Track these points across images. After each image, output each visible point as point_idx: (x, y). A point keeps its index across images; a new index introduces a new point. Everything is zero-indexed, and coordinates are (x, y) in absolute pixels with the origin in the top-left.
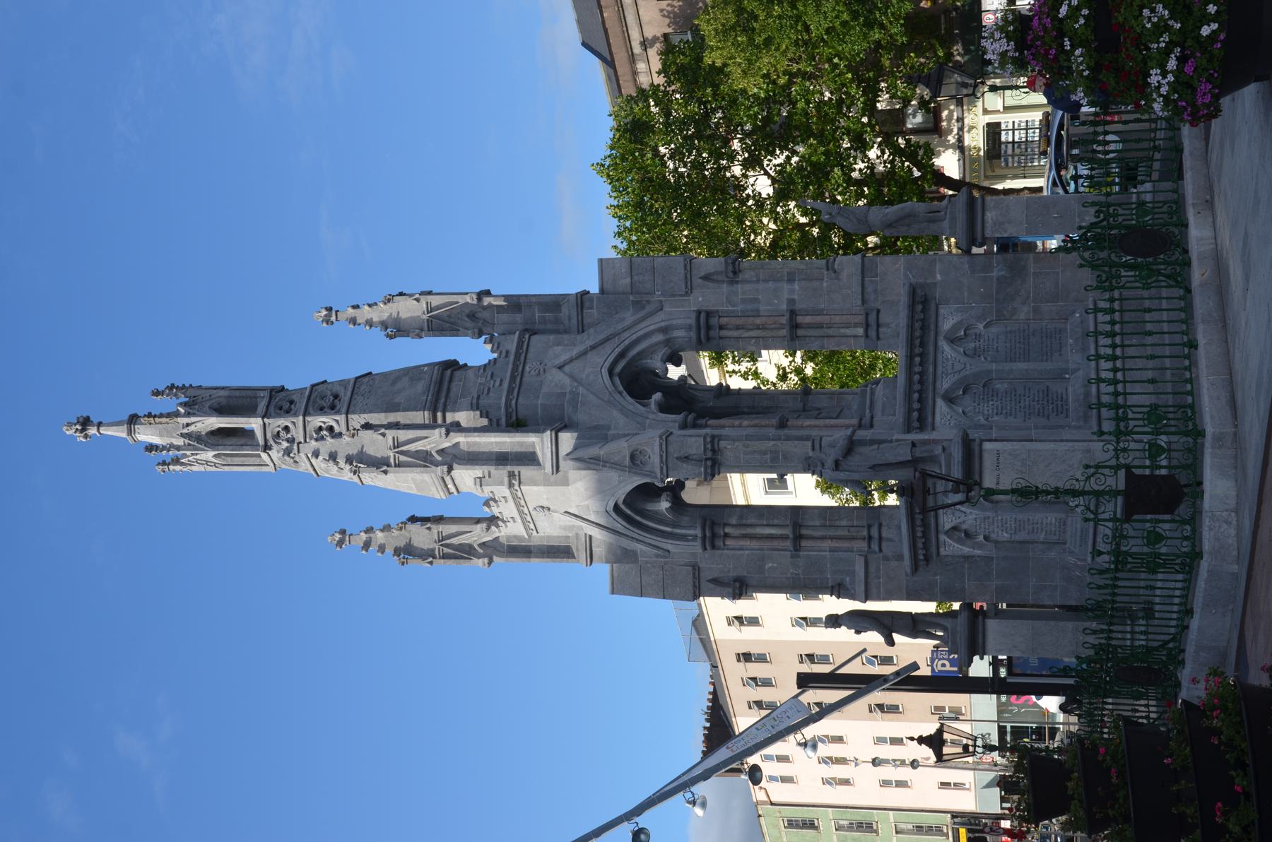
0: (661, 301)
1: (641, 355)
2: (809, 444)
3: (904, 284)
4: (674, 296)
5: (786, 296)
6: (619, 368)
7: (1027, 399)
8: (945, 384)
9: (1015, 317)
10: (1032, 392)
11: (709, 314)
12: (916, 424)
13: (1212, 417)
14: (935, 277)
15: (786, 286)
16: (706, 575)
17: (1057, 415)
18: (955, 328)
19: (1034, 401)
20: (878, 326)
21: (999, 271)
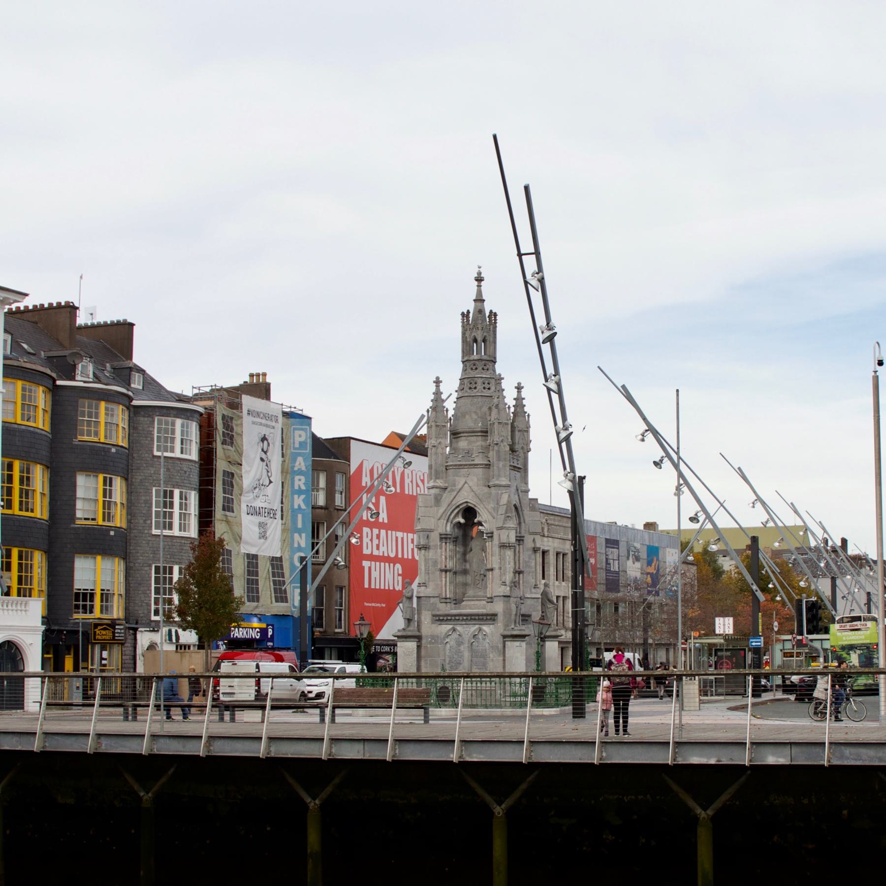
8: (459, 628)
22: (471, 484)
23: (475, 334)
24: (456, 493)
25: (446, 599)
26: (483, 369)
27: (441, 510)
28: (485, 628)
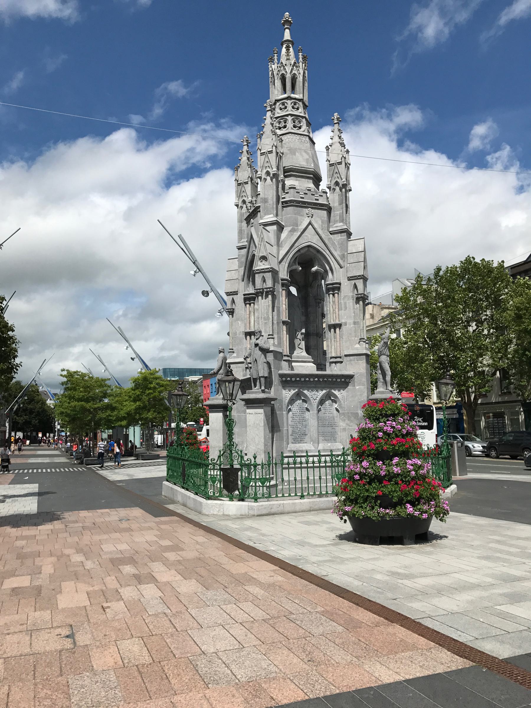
0: (344, 267)
2: (271, 333)
3: (354, 373)
4: (347, 272)
5: (348, 321)
6: (311, 250)
7: (301, 426)
9: (341, 421)
10: (304, 428)
11: (339, 289)
12: (284, 379)
13: (262, 505)
14: (357, 386)
15: (352, 321)
16: (235, 297)
17: (293, 439)
19: (300, 429)
21: (361, 413)
24: (299, 233)
27: (283, 252)
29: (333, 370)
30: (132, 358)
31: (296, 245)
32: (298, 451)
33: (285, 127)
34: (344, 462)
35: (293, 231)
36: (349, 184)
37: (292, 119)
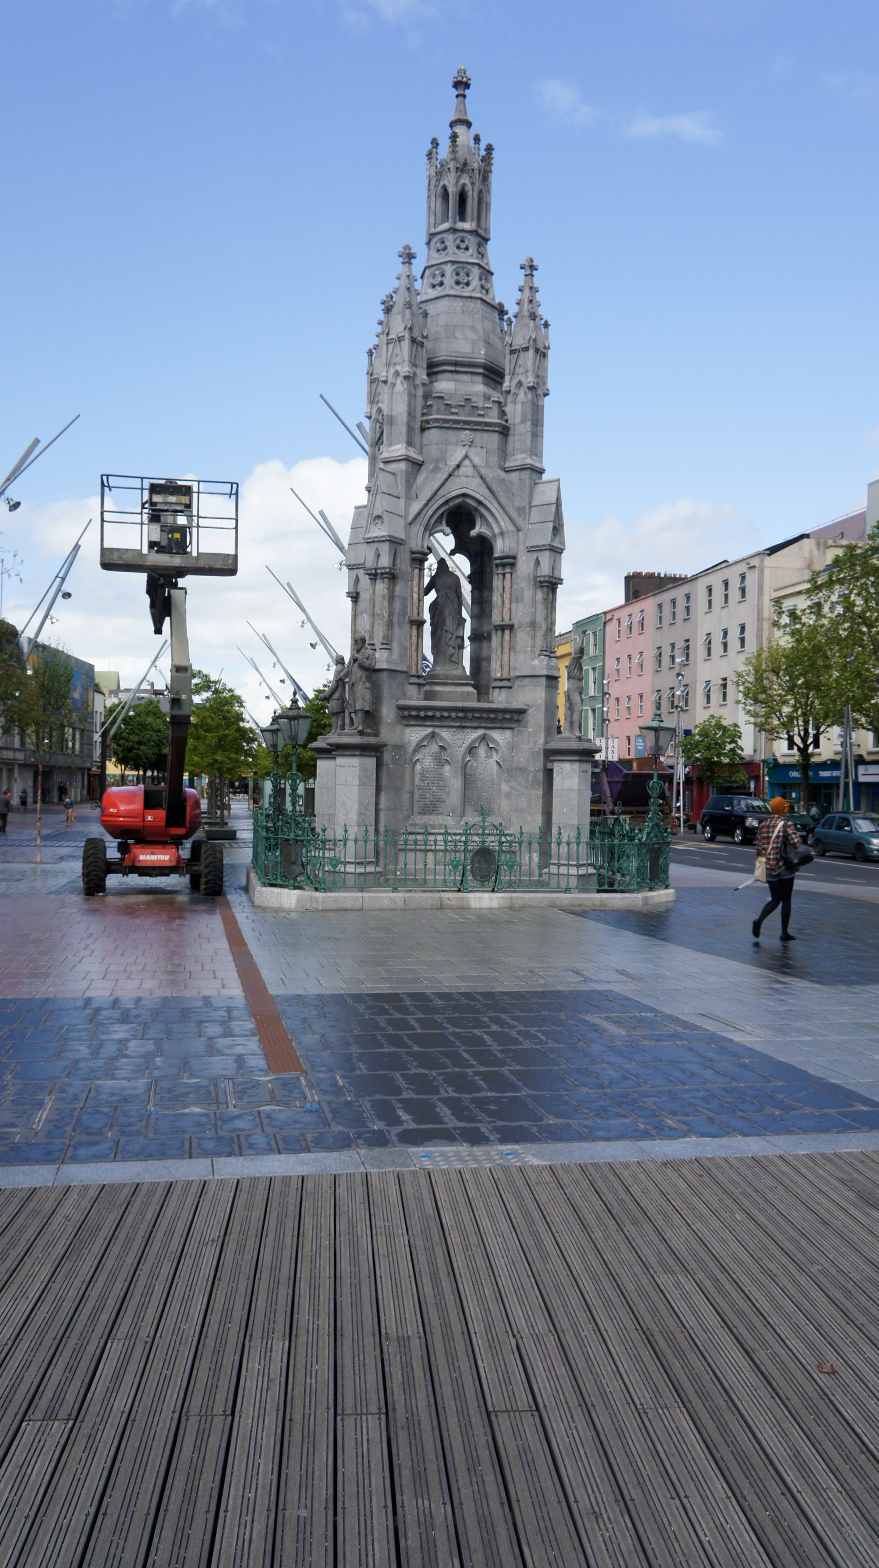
1: (482, 516)
6: (469, 501)
8: (445, 734)
11: (513, 565)
13: (330, 897)
18: (494, 741)
20: (500, 688)
22: (477, 460)
23: (446, 182)
25: (419, 677)
26: (458, 247)
27: (416, 507)
28: (496, 735)
29: (499, 699)
30: (311, 645)
31: (441, 492)
32: (433, 827)
33: (441, 284)
34: (465, 843)
35: (436, 469)
36: (545, 383)
37: (455, 270)
